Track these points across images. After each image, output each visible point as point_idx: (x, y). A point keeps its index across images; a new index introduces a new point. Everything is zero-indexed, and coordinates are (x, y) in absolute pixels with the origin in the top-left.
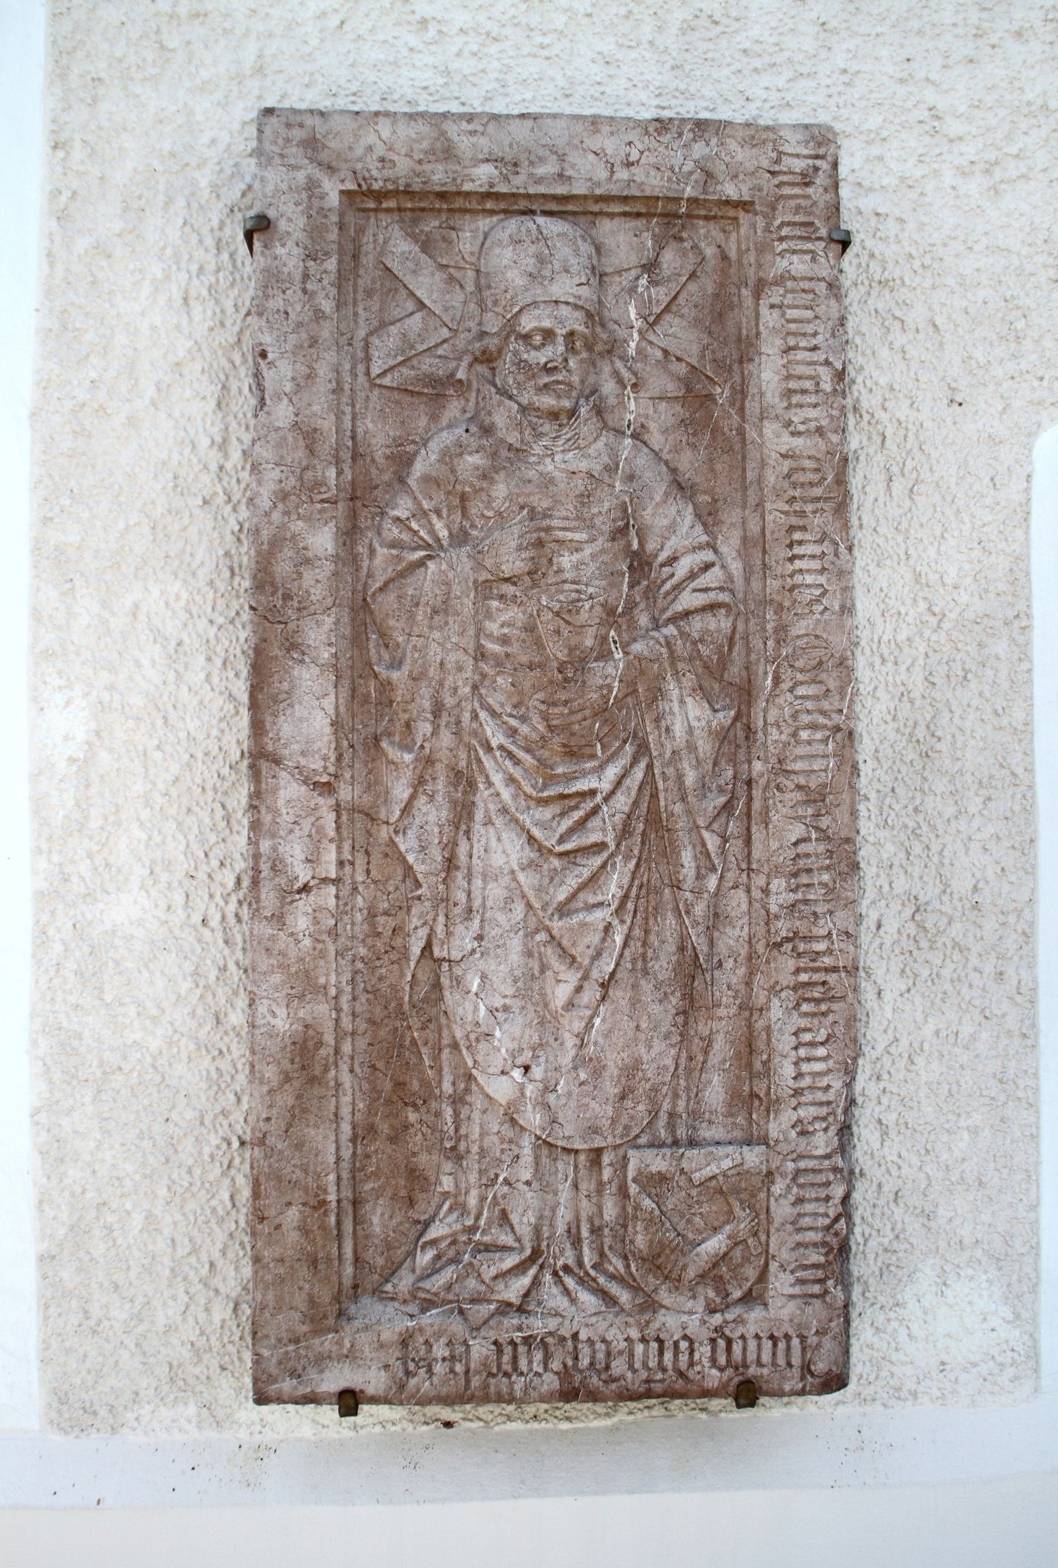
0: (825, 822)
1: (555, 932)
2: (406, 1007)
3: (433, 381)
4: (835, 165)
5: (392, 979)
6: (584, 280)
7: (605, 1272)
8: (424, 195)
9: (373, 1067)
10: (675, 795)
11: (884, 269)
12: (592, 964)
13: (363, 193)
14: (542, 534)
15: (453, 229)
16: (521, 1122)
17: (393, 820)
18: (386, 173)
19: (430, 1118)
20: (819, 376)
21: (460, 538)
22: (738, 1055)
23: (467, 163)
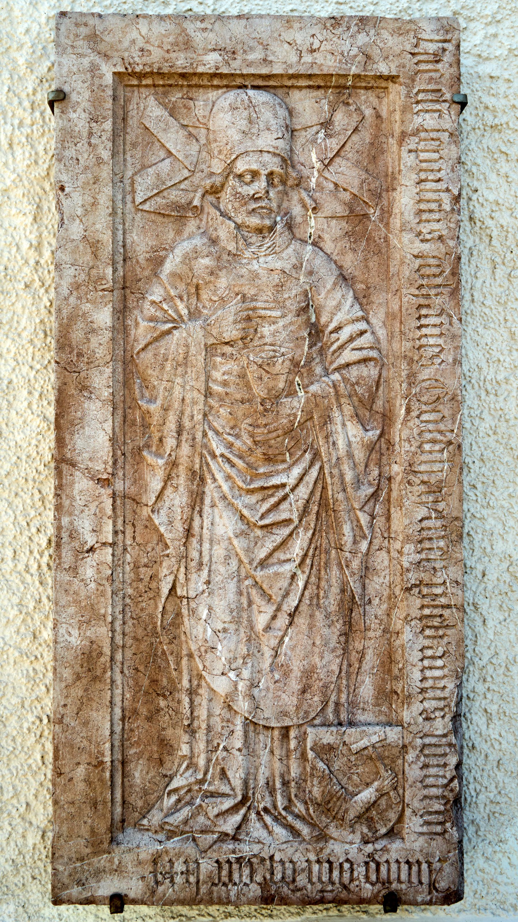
0: (441, 506)
1: (257, 579)
2: (159, 629)
3: (178, 207)
4: (458, 46)
5: (150, 610)
6: (280, 135)
7: (292, 813)
8: (170, 75)
9: (137, 670)
10: (338, 487)
11: (495, 117)
12: (283, 600)
13: (129, 74)
14: (251, 312)
15: (191, 99)
16: (235, 708)
17: (150, 504)
18: (145, 59)
19: (174, 705)
20: (441, 200)
21: (194, 314)
22: (382, 663)
23: (201, 52)
